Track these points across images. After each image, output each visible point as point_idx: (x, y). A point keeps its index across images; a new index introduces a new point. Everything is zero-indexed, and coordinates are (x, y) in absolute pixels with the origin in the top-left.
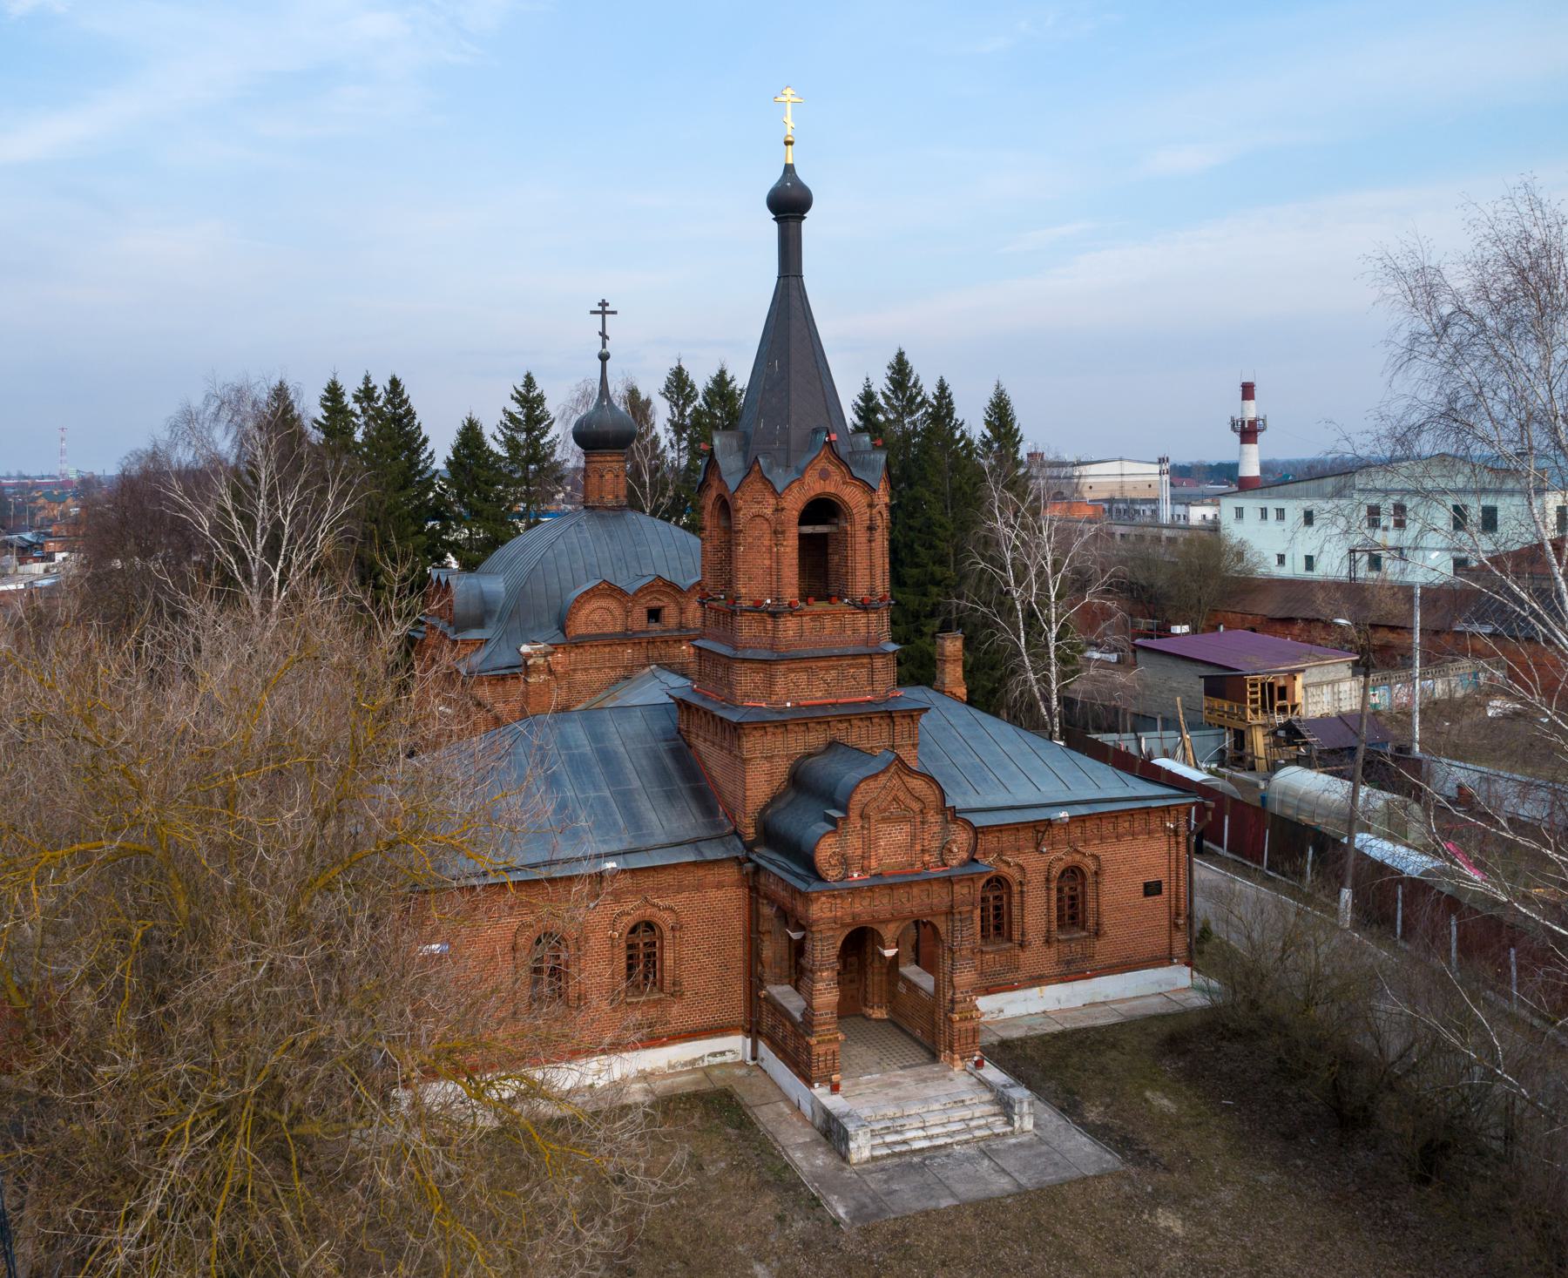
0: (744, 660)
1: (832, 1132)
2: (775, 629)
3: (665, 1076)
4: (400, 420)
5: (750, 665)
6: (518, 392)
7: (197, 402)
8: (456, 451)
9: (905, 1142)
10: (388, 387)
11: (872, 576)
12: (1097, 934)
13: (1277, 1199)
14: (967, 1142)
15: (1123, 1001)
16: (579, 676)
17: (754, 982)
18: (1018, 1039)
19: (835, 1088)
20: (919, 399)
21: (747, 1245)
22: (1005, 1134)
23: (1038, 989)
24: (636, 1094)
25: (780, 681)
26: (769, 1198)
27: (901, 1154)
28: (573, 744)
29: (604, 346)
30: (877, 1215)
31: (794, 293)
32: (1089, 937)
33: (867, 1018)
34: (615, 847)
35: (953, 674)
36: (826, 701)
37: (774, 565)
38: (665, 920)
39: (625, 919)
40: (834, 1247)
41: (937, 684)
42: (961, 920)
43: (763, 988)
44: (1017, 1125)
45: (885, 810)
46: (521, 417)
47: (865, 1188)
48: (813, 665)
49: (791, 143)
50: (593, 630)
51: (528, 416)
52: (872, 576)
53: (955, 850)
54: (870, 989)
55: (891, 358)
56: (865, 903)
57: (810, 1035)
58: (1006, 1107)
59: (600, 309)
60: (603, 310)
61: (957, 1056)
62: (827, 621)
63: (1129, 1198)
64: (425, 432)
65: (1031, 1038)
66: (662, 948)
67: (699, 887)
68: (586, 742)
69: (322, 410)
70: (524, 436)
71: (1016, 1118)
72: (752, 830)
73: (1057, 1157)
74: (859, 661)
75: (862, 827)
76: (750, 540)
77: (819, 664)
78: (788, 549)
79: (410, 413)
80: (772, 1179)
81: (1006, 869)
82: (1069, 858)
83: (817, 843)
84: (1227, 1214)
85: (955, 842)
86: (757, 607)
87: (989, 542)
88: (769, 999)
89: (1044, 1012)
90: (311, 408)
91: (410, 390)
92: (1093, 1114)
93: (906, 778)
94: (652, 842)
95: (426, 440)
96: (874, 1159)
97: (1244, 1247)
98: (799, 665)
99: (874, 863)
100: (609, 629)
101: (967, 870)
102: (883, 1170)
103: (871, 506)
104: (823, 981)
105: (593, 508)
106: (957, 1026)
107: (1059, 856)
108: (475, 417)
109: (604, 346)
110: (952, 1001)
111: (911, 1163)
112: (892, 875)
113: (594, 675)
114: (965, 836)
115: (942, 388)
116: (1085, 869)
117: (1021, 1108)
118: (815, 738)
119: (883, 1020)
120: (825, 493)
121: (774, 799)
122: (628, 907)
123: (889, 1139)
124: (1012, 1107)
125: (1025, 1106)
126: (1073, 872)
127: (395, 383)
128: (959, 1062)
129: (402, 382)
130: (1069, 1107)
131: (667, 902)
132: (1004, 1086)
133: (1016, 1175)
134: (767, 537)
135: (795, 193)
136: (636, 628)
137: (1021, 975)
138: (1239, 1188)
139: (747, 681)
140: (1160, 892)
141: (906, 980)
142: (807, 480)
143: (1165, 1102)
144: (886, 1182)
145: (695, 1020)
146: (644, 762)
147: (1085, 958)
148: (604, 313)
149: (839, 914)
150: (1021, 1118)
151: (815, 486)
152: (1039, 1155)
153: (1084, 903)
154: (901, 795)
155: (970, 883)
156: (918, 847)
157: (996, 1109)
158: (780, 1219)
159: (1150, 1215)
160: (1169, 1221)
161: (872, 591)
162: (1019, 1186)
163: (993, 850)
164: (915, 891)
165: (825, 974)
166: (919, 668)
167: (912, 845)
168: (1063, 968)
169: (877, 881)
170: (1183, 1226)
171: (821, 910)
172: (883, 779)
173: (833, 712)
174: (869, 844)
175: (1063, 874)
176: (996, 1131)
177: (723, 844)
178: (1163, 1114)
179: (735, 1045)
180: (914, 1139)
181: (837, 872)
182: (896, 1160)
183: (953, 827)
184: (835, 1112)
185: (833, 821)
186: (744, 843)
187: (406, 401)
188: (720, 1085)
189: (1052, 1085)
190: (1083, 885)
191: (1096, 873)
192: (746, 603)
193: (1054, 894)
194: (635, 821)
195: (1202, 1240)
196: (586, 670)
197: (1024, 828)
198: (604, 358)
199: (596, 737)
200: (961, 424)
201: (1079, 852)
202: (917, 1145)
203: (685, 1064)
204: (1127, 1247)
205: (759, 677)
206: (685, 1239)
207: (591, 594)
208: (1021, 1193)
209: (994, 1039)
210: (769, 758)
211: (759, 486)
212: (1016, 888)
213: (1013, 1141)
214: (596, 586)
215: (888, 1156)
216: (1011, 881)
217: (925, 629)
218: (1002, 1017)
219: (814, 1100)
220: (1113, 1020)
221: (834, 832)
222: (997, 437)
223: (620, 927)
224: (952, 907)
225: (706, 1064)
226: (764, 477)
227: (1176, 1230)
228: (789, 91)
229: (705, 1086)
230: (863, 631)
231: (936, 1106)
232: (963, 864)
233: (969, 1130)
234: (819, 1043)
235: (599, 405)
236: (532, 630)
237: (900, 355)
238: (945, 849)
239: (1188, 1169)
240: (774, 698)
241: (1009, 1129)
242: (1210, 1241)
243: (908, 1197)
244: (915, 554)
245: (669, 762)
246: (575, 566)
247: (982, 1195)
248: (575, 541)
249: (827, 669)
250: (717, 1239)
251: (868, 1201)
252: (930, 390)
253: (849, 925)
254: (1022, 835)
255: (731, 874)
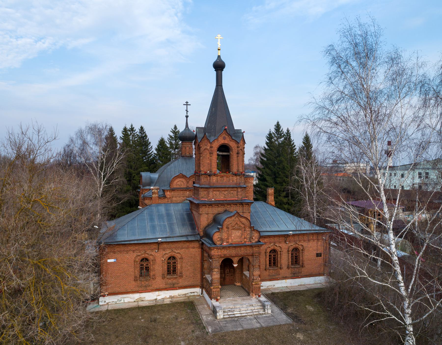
0: (202, 188)
1: (214, 311)
2: (210, 180)
3: (177, 297)
4: (143, 138)
5: (203, 189)
6: (173, 130)
7: (83, 128)
8: (158, 146)
9: (234, 314)
10: (140, 129)
11: (238, 166)
12: (302, 266)
13: (332, 332)
14: (251, 315)
15: (309, 285)
16: (174, 199)
17: (203, 274)
18: (277, 292)
19: (217, 300)
20: (283, 135)
21: (182, 337)
22: (263, 314)
23: (285, 280)
24: (167, 301)
25: (211, 193)
26: (192, 326)
27: (232, 317)
28: (160, 211)
29: (187, 114)
30: (219, 332)
31: (220, 90)
32: (300, 267)
33: (235, 285)
34: (162, 236)
35: (271, 199)
36: (223, 199)
37: (210, 162)
38: (178, 256)
39: (166, 255)
40: (205, 338)
41: (267, 201)
42: (256, 257)
43: (204, 275)
44: (266, 312)
45: (234, 227)
46: (173, 136)
47: (219, 325)
48: (221, 190)
49: (220, 50)
50: (178, 187)
51: (175, 136)
52: (238, 166)
53: (254, 238)
54: (236, 278)
55: (276, 123)
56: (228, 251)
57: (211, 286)
58: (264, 306)
59: (186, 104)
60: (187, 104)
61: (254, 294)
62: (225, 178)
63: (291, 330)
64: (150, 141)
65: (281, 292)
66: (177, 264)
67: (188, 248)
68: (164, 211)
69: (122, 134)
70: (174, 142)
71: (266, 310)
72: (202, 233)
73: (275, 320)
74: (234, 189)
75: (227, 231)
76: (204, 155)
77: (222, 189)
78: (214, 158)
79: (146, 136)
80: (195, 322)
81: (276, 247)
82: (295, 246)
83: (214, 234)
84: (317, 335)
85: (254, 236)
86: (206, 174)
87: (298, 172)
88: (205, 278)
89: (287, 286)
90: (119, 134)
91: (146, 130)
92: (289, 310)
93: (240, 218)
94: (175, 235)
95: (150, 143)
96: (224, 318)
97: (318, 343)
98: (216, 189)
99: (230, 241)
100: (183, 186)
101: (257, 244)
102: (226, 321)
103: (238, 147)
104: (216, 272)
105: (183, 156)
106: (254, 286)
107: (292, 245)
108: (163, 137)
109: (187, 114)
110: (253, 279)
111: (234, 320)
112: (235, 244)
113: (178, 199)
114: (257, 235)
115: (288, 131)
116: (299, 249)
117: (268, 307)
118: (220, 209)
119: (239, 286)
120: (224, 143)
121: (208, 225)
122: (167, 252)
123: (229, 313)
124: (265, 307)
125: (269, 307)
126: (296, 249)
127: (142, 128)
128: (255, 296)
129: (144, 128)
130: (284, 309)
131: (178, 252)
132: (264, 302)
133: (262, 324)
134: (208, 155)
135: (220, 63)
136: (190, 186)
137: (280, 276)
138: (323, 329)
139: (202, 193)
140: (321, 256)
141: (245, 275)
142: (219, 139)
143: (311, 308)
144: (225, 324)
145: (186, 283)
146: (179, 217)
147: (299, 273)
148: (187, 105)
149: (220, 254)
150: (267, 310)
151: (221, 141)
152: (270, 319)
153: (299, 258)
154: (238, 223)
155: (258, 247)
156: (243, 237)
157: (261, 307)
158: (193, 331)
159: (295, 334)
160: (300, 336)
161: (238, 170)
162: (262, 326)
163: (272, 242)
164: (242, 249)
165: (216, 270)
166: (280, 205)
167: (242, 236)
168: (293, 275)
169: (231, 245)
170: (303, 337)
171: (214, 252)
172: (233, 218)
173: (225, 202)
174: (229, 235)
175: (293, 249)
176: (260, 313)
177: (195, 237)
178: (309, 311)
179: (198, 291)
180: (237, 314)
181: (219, 242)
182: (230, 319)
183: (253, 232)
184: (215, 306)
185: (218, 229)
186: (200, 236)
187: (145, 132)
188: (191, 300)
189: (281, 303)
190: (299, 253)
191: (302, 250)
192: (203, 173)
193: (290, 255)
194: (172, 230)
195: (308, 341)
196: (176, 197)
197: (282, 237)
198: (187, 117)
199: (167, 210)
200: (293, 141)
201: (297, 244)
202: (237, 315)
203: (183, 295)
204: (286, 342)
205: (205, 192)
206: (165, 335)
207: (177, 177)
208: (262, 329)
209: (270, 292)
210: (208, 214)
211: (206, 141)
212: (279, 253)
213: (265, 316)
214: (179, 175)
215: (228, 318)
216: (278, 251)
217: (282, 195)
218: (274, 287)
219: (212, 303)
220: (305, 289)
221: (219, 231)
222: (306, 146)
223: (165, 257)
224: (253, 254)
225: (189, 295)
226: (207, 138)
227: (301, 338)
228: (219, 35)
229: (187, 300)
230: (235, 181)
231: (245, 306)
232: (256, 242)
233: (253, 312)
234: (214, 288)
235: (185, 129)
236: (162, 186)
237: (278, 123)
238: (251, 238)
239: (311, 324)
240: (209, 198)
241: (264, 312)
242: (309, 341)
243: (230, 327)
244: (279, 175)
245: (185, 217)
246: (175, 170)
247: (250, 328)
248: (177, 164)
249: (225, 191)
250: (174, 335)
251: (218, 328)
252: (285, 131)
253: (223, 257)
254: (281, 238)
255: (197, 245)
